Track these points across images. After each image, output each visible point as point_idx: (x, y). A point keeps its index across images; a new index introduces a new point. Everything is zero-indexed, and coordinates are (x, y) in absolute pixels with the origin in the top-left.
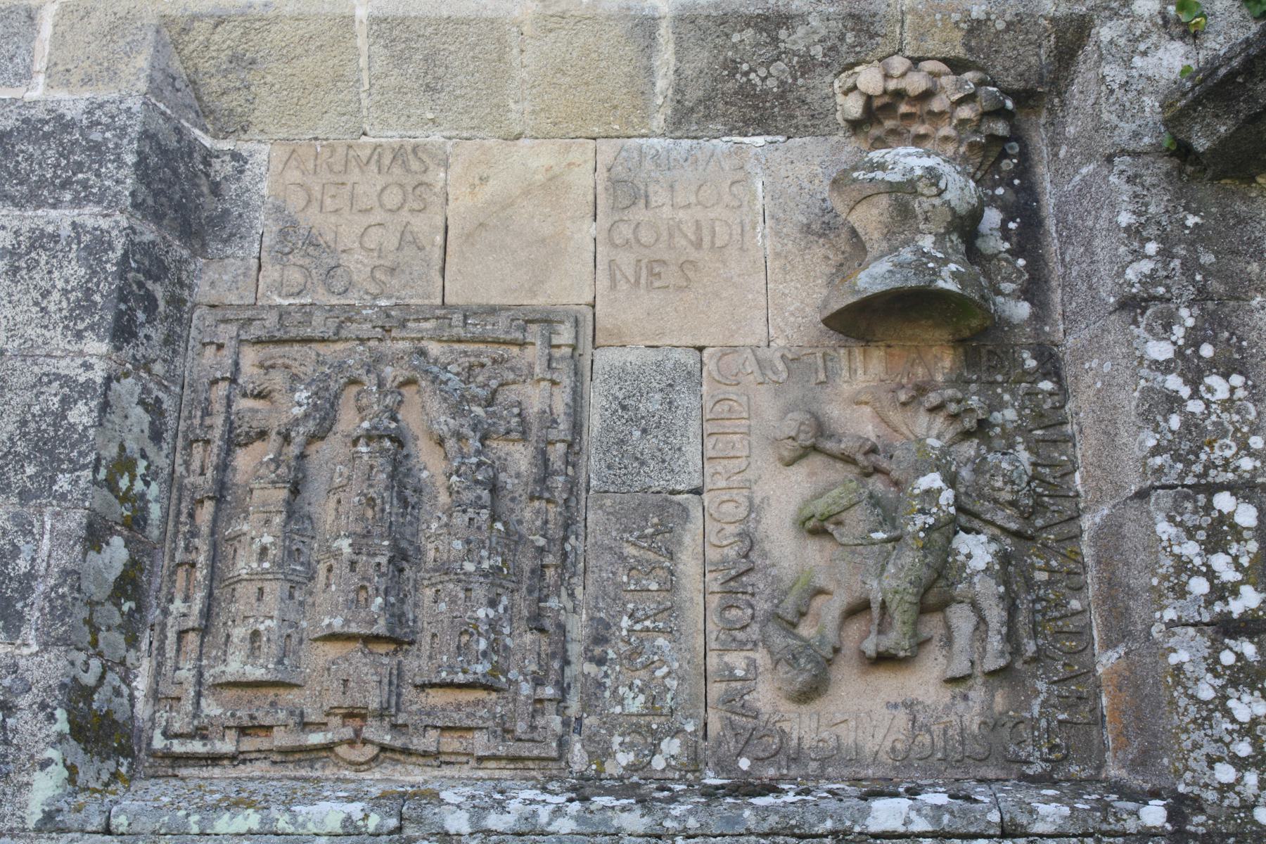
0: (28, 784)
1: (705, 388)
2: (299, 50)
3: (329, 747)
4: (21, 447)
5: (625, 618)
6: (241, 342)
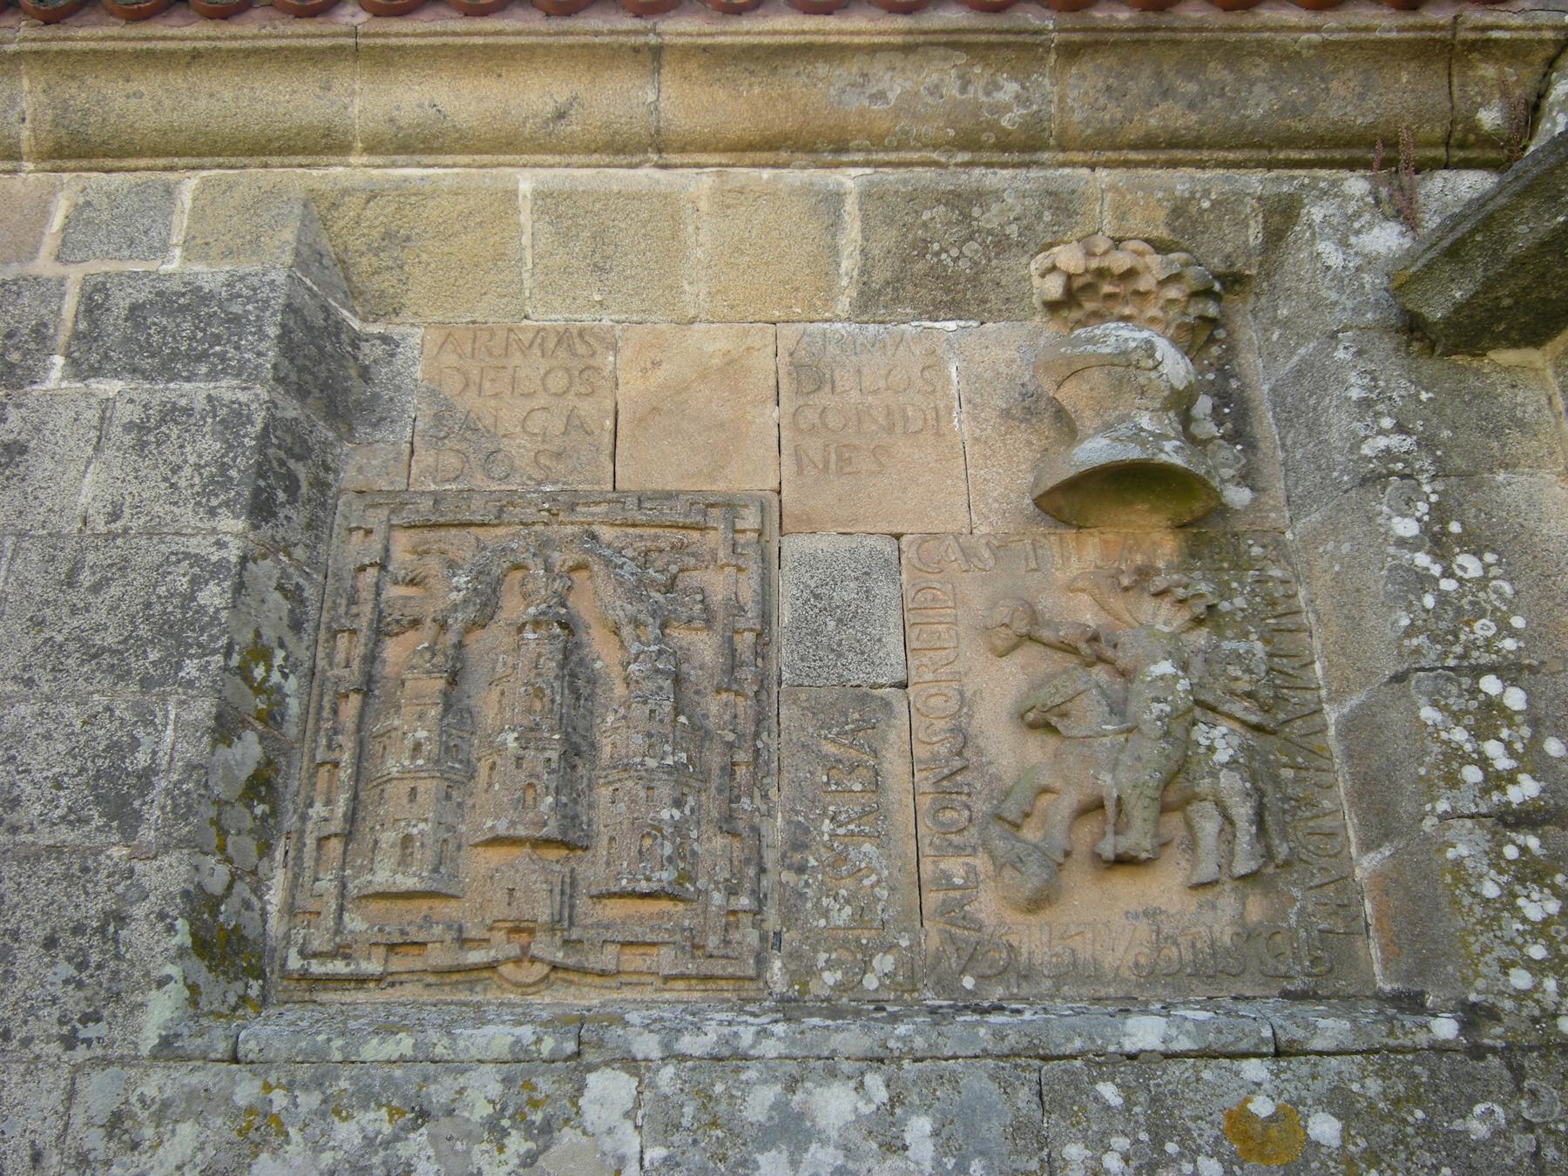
0: (142, 1005)
1: (904, 576)
2: (457, 227)
3: (491, 966)
4: (144, 631)
5: (827, 821)
6: (392, 527)
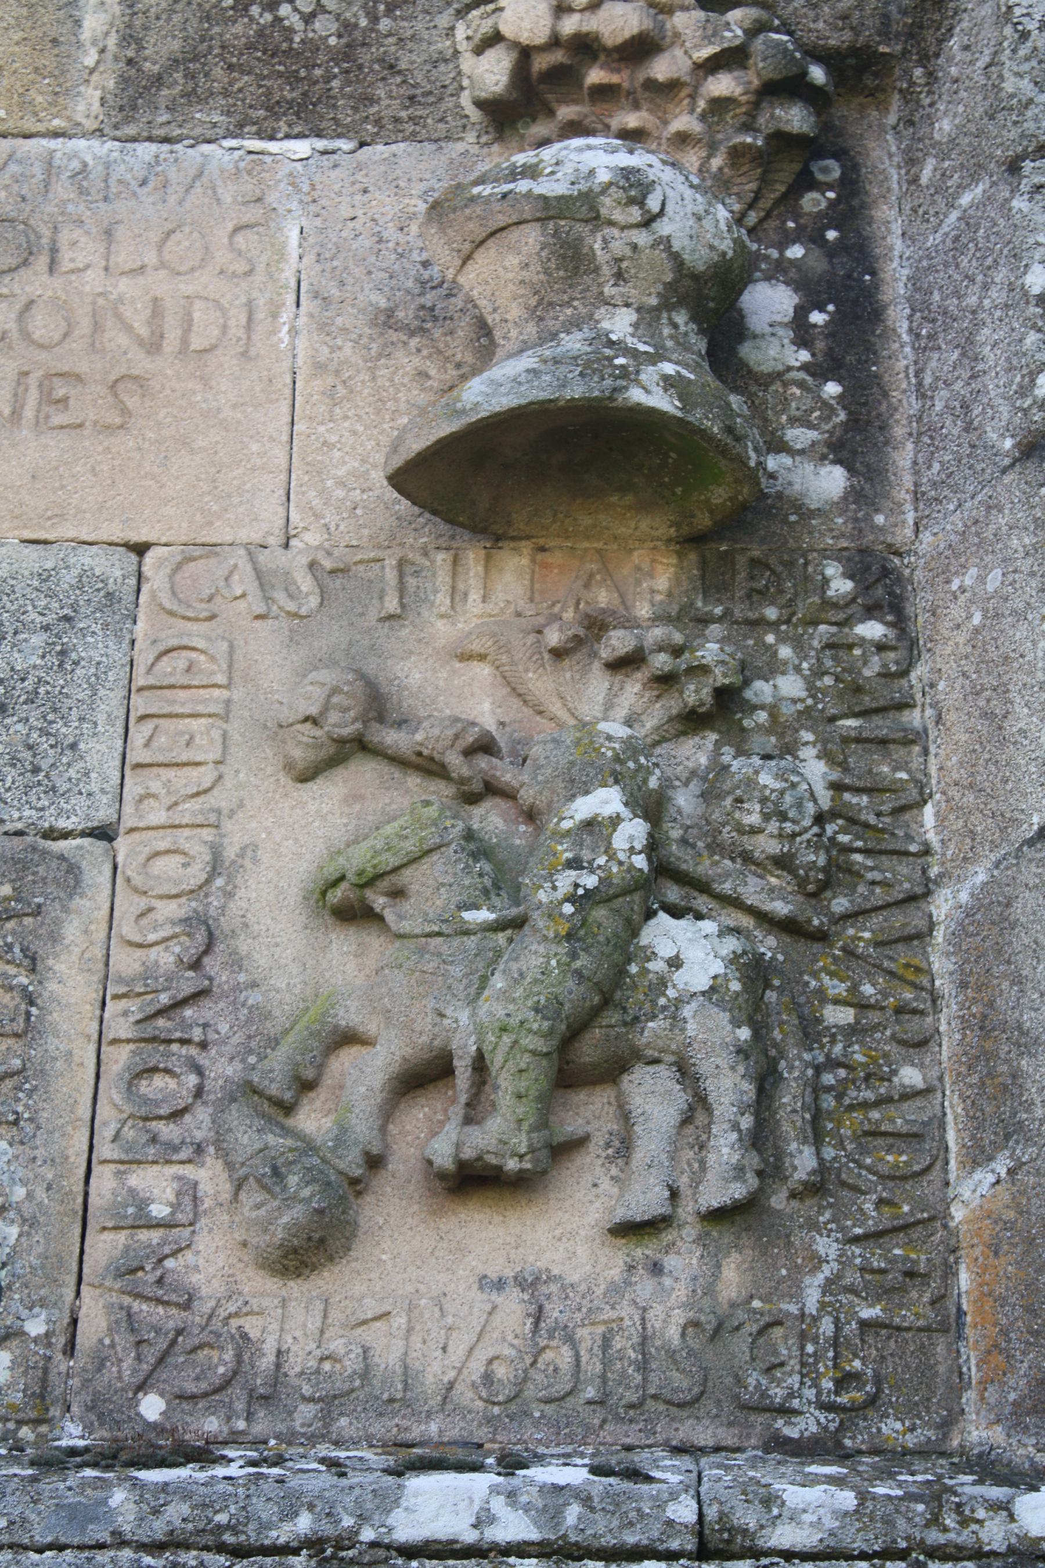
1: (141, 626)
